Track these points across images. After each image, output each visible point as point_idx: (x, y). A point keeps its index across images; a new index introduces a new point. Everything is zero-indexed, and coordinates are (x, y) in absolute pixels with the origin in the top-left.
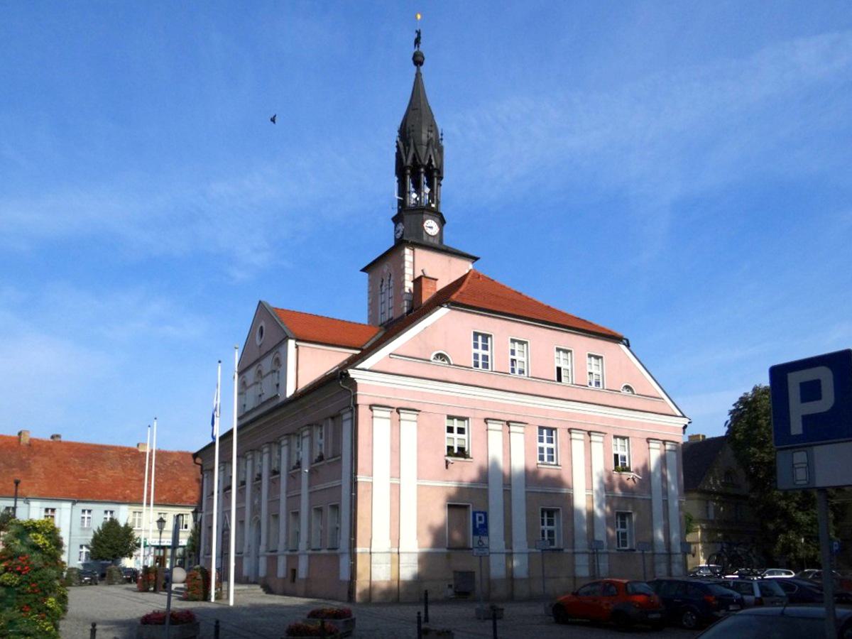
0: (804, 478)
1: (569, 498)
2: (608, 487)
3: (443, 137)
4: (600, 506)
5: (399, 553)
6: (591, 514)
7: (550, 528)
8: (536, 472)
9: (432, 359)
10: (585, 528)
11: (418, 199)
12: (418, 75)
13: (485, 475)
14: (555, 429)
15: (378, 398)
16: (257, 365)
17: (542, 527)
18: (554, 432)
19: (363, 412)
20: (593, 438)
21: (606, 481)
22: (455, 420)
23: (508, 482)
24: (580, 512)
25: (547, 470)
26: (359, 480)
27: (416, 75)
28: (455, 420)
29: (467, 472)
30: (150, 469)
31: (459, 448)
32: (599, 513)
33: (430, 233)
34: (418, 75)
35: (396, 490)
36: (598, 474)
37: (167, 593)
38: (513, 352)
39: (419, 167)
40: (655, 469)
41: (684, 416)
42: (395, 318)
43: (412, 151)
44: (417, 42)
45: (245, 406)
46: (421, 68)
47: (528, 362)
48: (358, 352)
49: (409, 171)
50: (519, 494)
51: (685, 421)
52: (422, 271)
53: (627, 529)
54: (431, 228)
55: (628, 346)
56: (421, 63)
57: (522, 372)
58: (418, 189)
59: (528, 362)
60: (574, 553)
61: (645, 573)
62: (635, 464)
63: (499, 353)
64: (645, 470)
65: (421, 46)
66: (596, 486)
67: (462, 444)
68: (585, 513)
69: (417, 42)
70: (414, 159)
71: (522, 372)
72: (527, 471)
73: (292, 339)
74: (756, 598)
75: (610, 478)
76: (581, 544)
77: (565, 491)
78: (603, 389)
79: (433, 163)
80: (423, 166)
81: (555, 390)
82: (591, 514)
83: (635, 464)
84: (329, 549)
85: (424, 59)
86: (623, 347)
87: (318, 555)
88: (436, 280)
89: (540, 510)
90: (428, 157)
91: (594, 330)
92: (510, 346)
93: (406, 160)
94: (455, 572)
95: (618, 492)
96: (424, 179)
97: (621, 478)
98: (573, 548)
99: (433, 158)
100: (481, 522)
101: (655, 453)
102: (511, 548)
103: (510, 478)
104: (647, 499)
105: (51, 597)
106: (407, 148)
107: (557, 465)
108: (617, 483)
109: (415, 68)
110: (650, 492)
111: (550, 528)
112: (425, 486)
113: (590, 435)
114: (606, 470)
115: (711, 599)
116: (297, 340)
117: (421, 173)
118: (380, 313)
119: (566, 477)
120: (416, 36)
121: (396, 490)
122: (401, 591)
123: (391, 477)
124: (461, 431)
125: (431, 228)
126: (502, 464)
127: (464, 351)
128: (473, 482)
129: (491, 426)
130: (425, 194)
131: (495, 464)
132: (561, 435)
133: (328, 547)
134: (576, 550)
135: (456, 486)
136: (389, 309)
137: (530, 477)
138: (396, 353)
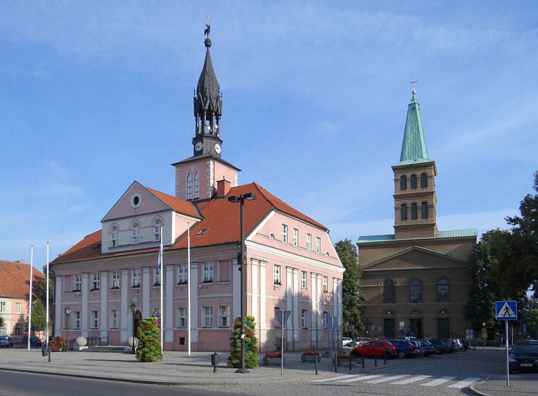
1: (311, 306)
3: (222, 95)
4: (320, 310)
5: (260, 330)
8: (302, 294)
9: (269, 236)
11: (211, 131)
12: (207, 53)
14: (306, 272)
16: (133, 219)
17: (212, 316)
18: (305, 274)
19: (248, 261)
20: (295, 272)
21: (321, 298)
25: (305, 294)
26: (248, 295)
27: (207, 53)
34: (207, 53)
37: (41, 350)
39: (212, 112)
42: (200, 199)
43: (209, 102)
44: (207, 31)
45: (114, 241)
46: (209, 48)
47: (287, 236)
48: (200, 220)
49: (205, 113)
52: (224, 176)
54: (218, 149)
58: (211, 124)
59: (287, 236)
60: (312, 330)
61: (317, 341)
62: (330, 290)
63: (292, 234)
65: (209, 35)
69: (207, 31)
70: (209, 106)
73: (174, 211)
74: (447, 347)
76: (314, 328)
78: (298, 246)
80: (214, 111)
82: (317, 313)
83: (330, 290)
84: (219, 327)
87: (210, 330)
88: (230, 183)
89: (301, 310)
93: (205, 107)
94: (277, 339)
95: (325, 303)
96: (214, 117)
98: (311, 328)
99: (219, 108)
102: (287, 327)
105: (497, 332)
106: (205, 98)
107: (306, 289)
109: (206, 48)
113: (293, 270)
115: (411, 347)
116: (176, 212)
117: (213, 115)
118: (186, 193)
120: (206, 28)
122: (262, 347)
125: (218, 149)
127: (280, 234)
130: (215, 128)
132: (283, 269)
133: (177, 327)
134: (312, 329)
136: (195, 192)
137: (300, 295)
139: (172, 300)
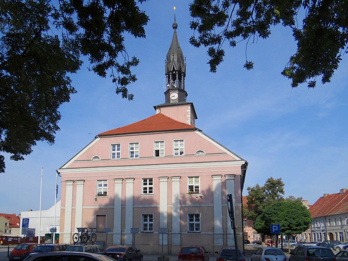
0: (127, 184)
2: (182, 202)
6: (170, 216)
7: (151, 223)
10: (166, 221)
12: (175, 32)
13: (112, 202)
15: (69, 178)
22: (194, 178)
23: (123, 203)
24: (162, 214)
28: (194, 178)
29: (104, 201)
30: (190, 218)
31: (104, 192)
32: (174, 214)
33: (173, 99)
34: (175, 32)
35: (73, 211)
36: (175, 196)
38: (132, 149)
40: (217, 188)
41: (242, 160)
50: (129, 208)
51: (243, 163)
53: (200, 222)
55: (200, 131)
56: (176, 28)
57: (137, 156)
64: (209, 190)
66: (173, 201)
67: (105, 190)
68: (166, 215)
71: (137, 156)
72: (134, 197)
75: (184, 197)
77: (154, 205)
79: (175, 68)
81: (156, 160)
82: (170, 216)
85: (177, 26)
86: (197, 132)
90: (173, 67)
91: (186, 128)
92: (131, 146)
97: (191, 197)
99: (175, 67)
100: (275, 230)
101: (216, 182)
103: (125, 201)
104: (212, 206)
108: (188, 200)
110: (212, 202)
111: (151, 223)
112: (86, 208)
114: (181, 193)
119: (155, 198)
121: (73, 211)
123: (125, 208)
124: (106, 185)
126: (120, 196)
128: (107, 205)
129: (214, 178)
131: (116, 196)
135: (99, 207)
137: (135, 200)
138: (76, 160)
139: (221, 206)
